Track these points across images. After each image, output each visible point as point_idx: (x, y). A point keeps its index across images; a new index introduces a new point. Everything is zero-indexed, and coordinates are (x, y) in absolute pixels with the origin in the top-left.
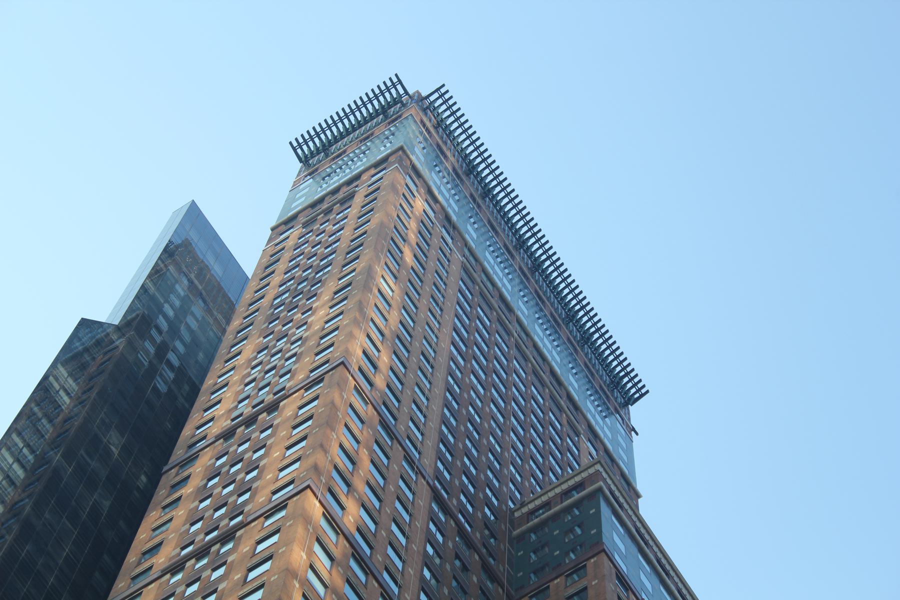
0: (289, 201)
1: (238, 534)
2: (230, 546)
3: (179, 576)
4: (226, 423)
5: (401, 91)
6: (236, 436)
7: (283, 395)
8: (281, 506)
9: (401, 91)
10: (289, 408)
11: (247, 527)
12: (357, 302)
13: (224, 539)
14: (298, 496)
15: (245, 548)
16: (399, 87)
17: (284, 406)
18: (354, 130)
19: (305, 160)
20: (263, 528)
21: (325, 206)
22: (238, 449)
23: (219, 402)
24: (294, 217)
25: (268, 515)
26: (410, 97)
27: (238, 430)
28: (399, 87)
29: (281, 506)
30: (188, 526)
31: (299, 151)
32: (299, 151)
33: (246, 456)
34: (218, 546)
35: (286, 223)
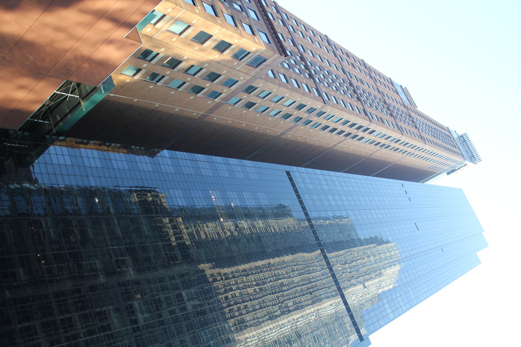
0: (397, 84)
1: (312, 80)
2: (307, 76)
3: (299, 59)
4: (355, 85)
5: (477, 161)
6: (385, 105)
7: (395, 118)
8: (320, 95)
9: (477, 161)
10: (359, 104)
11: (314, 83)
12: (184, 70)
13: (311, 76)
14: (322, 101)
15: (355, 104)
16: (479, 161)
17: (359, 103)
18: (469, 149)
19: (462, 136)
20: (312, 87)
21: (454, 141)
22: (293, 60)
23: (389, 99)
24: (451, 133)
25: (317, 90)
26: (227, 319)
27: (352, 87)
28: (479, 161)
29: (320, 95)
30: (327, 70)
31: (464, 135)
32: (464, 135)
33: (326, 80)
34: (308, 72)
35: (449, 131)
